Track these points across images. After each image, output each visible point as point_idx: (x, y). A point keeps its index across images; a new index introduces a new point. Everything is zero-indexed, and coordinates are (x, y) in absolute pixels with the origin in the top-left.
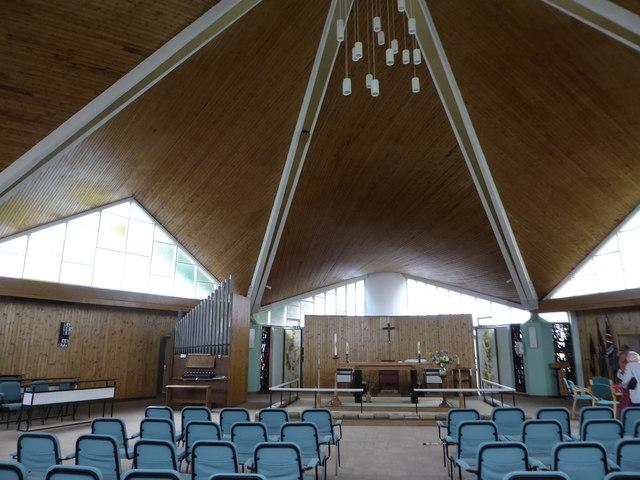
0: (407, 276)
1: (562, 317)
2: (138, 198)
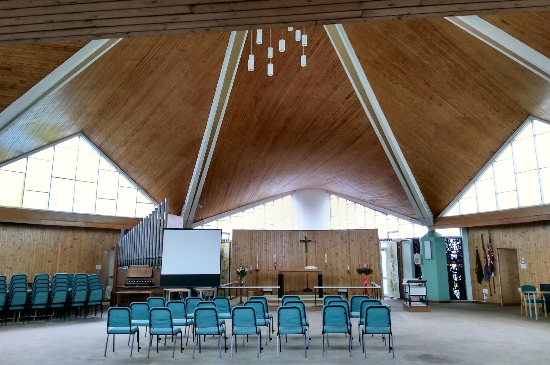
0: (330, 192)
1: (454, 232)
2: (84, 133)
